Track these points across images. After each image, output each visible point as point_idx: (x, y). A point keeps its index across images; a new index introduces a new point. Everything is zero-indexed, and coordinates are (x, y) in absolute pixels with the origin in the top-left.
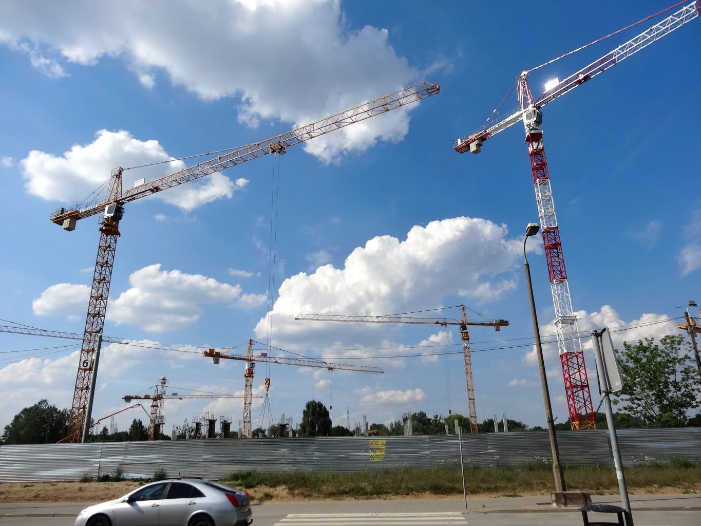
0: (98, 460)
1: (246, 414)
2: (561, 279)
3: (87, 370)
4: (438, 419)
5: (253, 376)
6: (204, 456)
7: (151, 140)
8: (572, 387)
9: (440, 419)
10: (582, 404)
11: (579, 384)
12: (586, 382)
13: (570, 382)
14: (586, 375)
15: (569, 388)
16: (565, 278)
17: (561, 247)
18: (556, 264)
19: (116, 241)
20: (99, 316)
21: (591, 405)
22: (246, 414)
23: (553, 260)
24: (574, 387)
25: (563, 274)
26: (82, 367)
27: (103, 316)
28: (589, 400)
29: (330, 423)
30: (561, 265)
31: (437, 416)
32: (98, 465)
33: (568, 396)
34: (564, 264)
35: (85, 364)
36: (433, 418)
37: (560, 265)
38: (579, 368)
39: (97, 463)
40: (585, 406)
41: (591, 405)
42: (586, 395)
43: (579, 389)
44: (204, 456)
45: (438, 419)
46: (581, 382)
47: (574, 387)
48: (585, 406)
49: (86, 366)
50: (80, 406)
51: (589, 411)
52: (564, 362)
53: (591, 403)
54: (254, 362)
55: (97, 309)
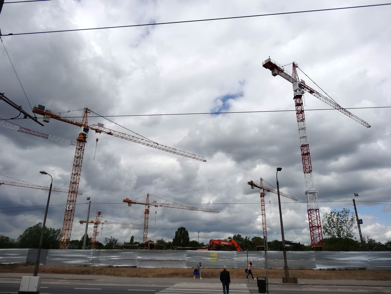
0: (92, 257)
1: (145, 233)
2: (309, 171)
3: (70, 210)
4: (247, 239)
5: (149, 213)
6: (138, 257)
7: (1, 11)
8: (312, 226)
9: (249, 239)
10: (317, 236)
11: (317, 225)
12: (320, 225)
13: (312, 224)
14: (320, 221)
15: (311, 227)
16: (311, 171)
17: (309, 155)
18: (307, 163)
19: (84, 145)
20: (76, 184)
21: (322, 236)
22: (145, 233)
23: (305, 161)
24: (314, 227)
25: (311, 169)
26: (68, 209)
27: (78, 183)
28: (319, 216)
29: (189, 239)
30: (310, 164)
31: (247, 237)
32: (92, 259)
33: (311, 231)
34: (311, 163)
35: (69, 208)
36: (245, 238)
37: (309, 164)
38: (317, 217)
39: (91, 258)
40: (319, 236)
41: (322, 236)
42: (318, 214)
43: (316, 228)
44: (138, 257)
45: (247, 239)
46: (318, 225)
47: (314, 227)
48: (319, 236)
49: (70, 208)
50: (66, 228)
51: (321, 239)
52: (309, 214)
53: (319, 217)
54: (149, 206)
55: (75, 180)
